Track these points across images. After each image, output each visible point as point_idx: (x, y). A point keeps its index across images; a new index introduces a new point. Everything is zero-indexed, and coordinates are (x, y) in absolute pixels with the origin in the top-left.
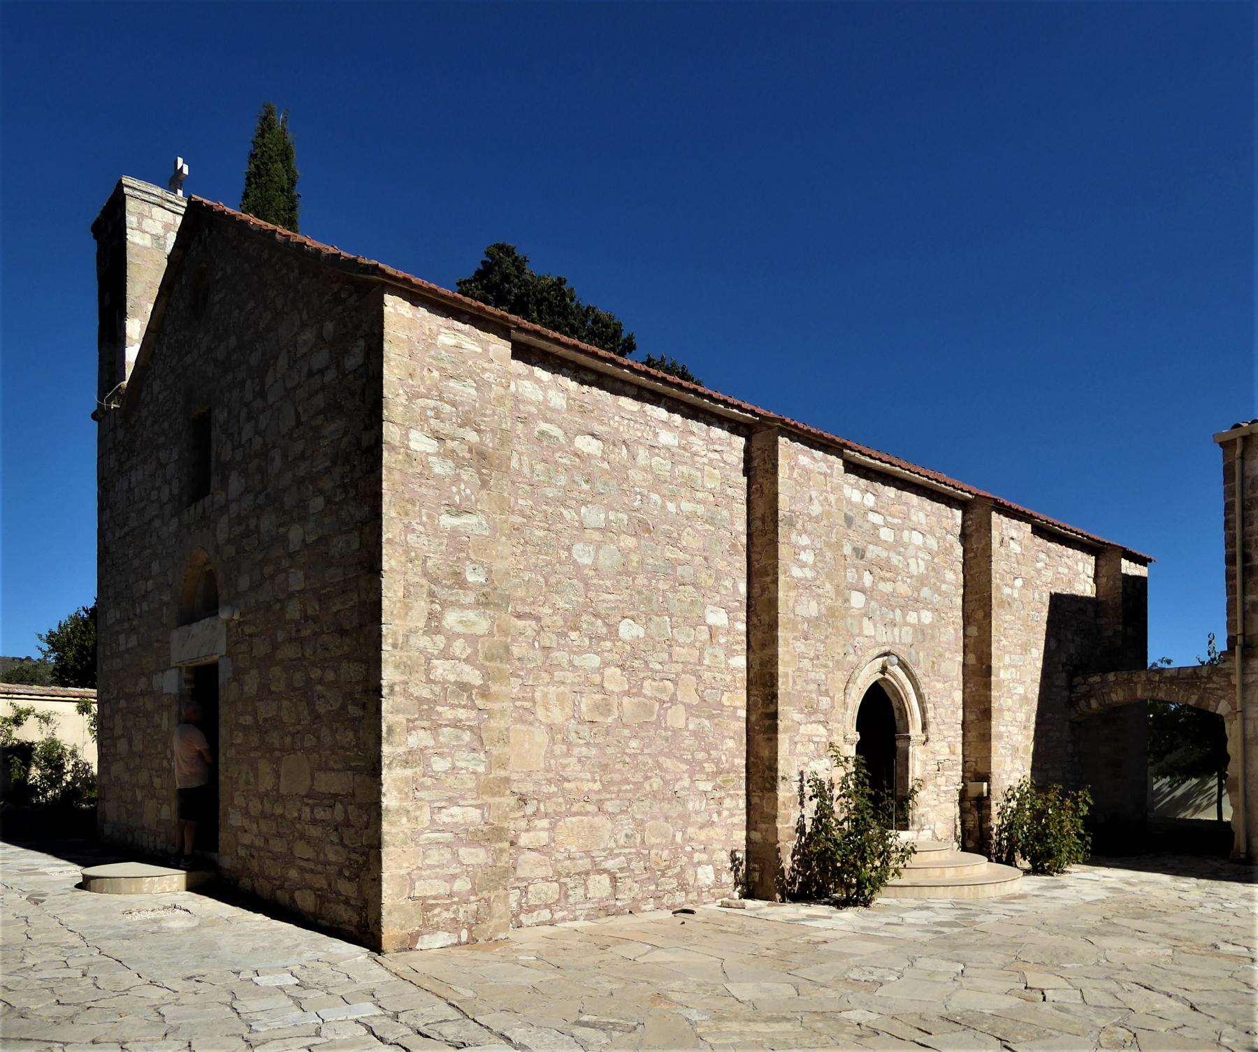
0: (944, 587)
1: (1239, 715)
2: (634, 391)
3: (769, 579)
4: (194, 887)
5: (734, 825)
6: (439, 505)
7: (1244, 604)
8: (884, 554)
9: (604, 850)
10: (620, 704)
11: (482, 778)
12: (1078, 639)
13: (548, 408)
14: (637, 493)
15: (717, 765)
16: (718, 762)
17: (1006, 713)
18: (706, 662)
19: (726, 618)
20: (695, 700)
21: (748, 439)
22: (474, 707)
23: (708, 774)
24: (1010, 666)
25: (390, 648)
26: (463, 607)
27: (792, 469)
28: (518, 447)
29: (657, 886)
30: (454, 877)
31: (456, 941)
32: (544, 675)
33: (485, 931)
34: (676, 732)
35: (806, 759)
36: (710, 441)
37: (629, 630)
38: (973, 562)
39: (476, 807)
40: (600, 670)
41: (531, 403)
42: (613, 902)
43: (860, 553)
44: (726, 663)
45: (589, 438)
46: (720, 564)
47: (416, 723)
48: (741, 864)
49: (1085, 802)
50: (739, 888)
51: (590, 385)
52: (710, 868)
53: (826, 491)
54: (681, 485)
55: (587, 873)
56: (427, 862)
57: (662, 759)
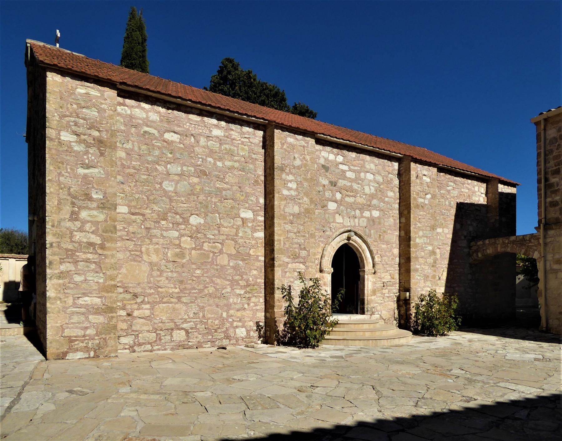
0: (386, 199)
1: (543, 258)
2: (198, 112)
4: (26, 334)
5: (257, 310)
6: (77, 164)
7: (545, 203)
8: (349, 184)
9: (181, 319)
10: (190, 254)
11: (101, 285)
12: (475, 224)
13: (149, 121)
14: (199, 158)
15: (247, 282)
16: (247, 281)
17: (420, 259)
18: (240, 235)
19: (252, 215)
20: (234, 252)
21: (265, 132)
22: (96, 253)
23: (241, 286)
24: (423, 236)
25: (50, 227)
26: (90, 209)
27: (283, 144)
28: (132, 139)
29: (213, 336)
30: (86, 328)
31: (88, 356)
32: (146, 240)
33: (104, 352)
35: (292, 280)
36: (242, 133)
37: (194, 220)
38: (403, 187)
39: (98, 297)
40: (179, 238)
41: (140, 119)
42: (187, 343)
43: (333, 184)
44: (252, 235)
45: (172, 134)
46: (248, 189)
47: (65, 260)
48: (262, 328)
49: (455, 301)
50: (262, 339)
51: (173, 109)
52: (244, 329)
53: (304, 154)
54: (225, 154)
55: (172, 329)
56: (71, 321)
57: (214, 279)
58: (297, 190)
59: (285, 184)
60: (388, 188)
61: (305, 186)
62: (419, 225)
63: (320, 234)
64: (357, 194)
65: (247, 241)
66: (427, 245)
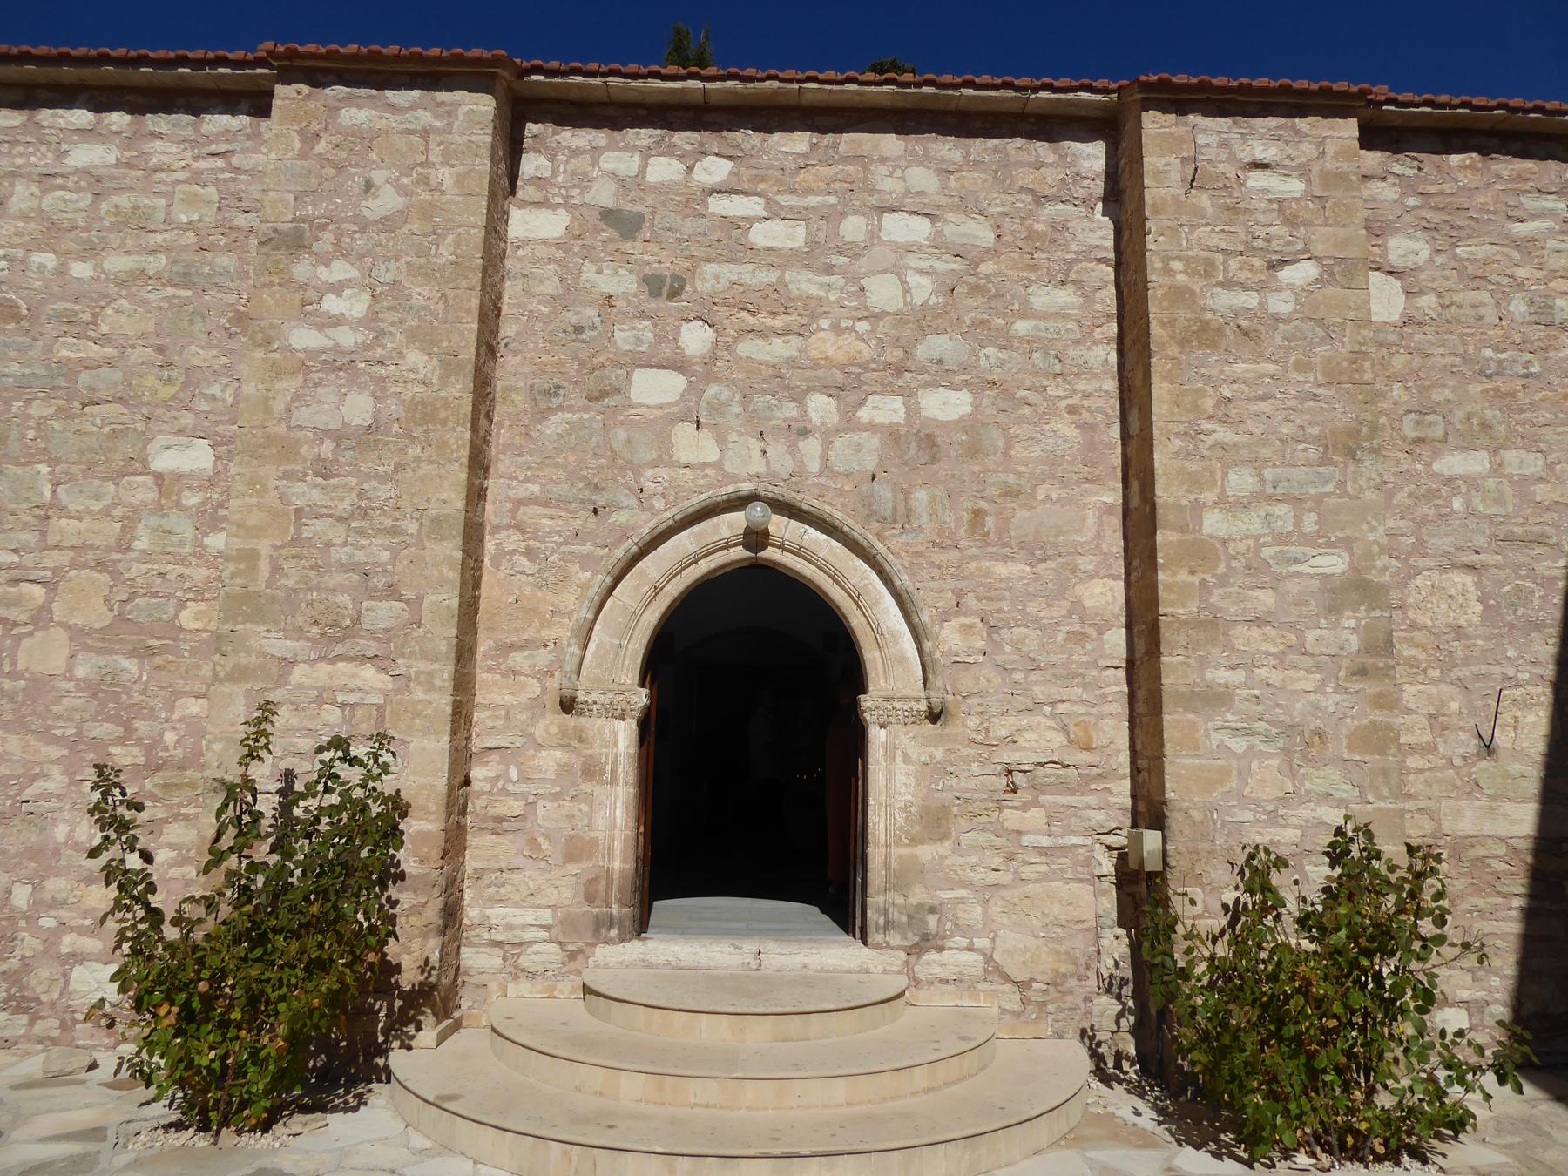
0: (1022, 327)
8: (766, 277)
15: (149, 750)
18: (142, 544)
24: (1259, 497)
34: (39, 684)
46: (198, 355)
58: (371, 320)
59: (304, 303)
60: (1033, 268)
61: (418, 301)
62: (1223, 434)
63: (576, 524)
64: (814, 316)
65: (173, 570)
66: (1295, 550)
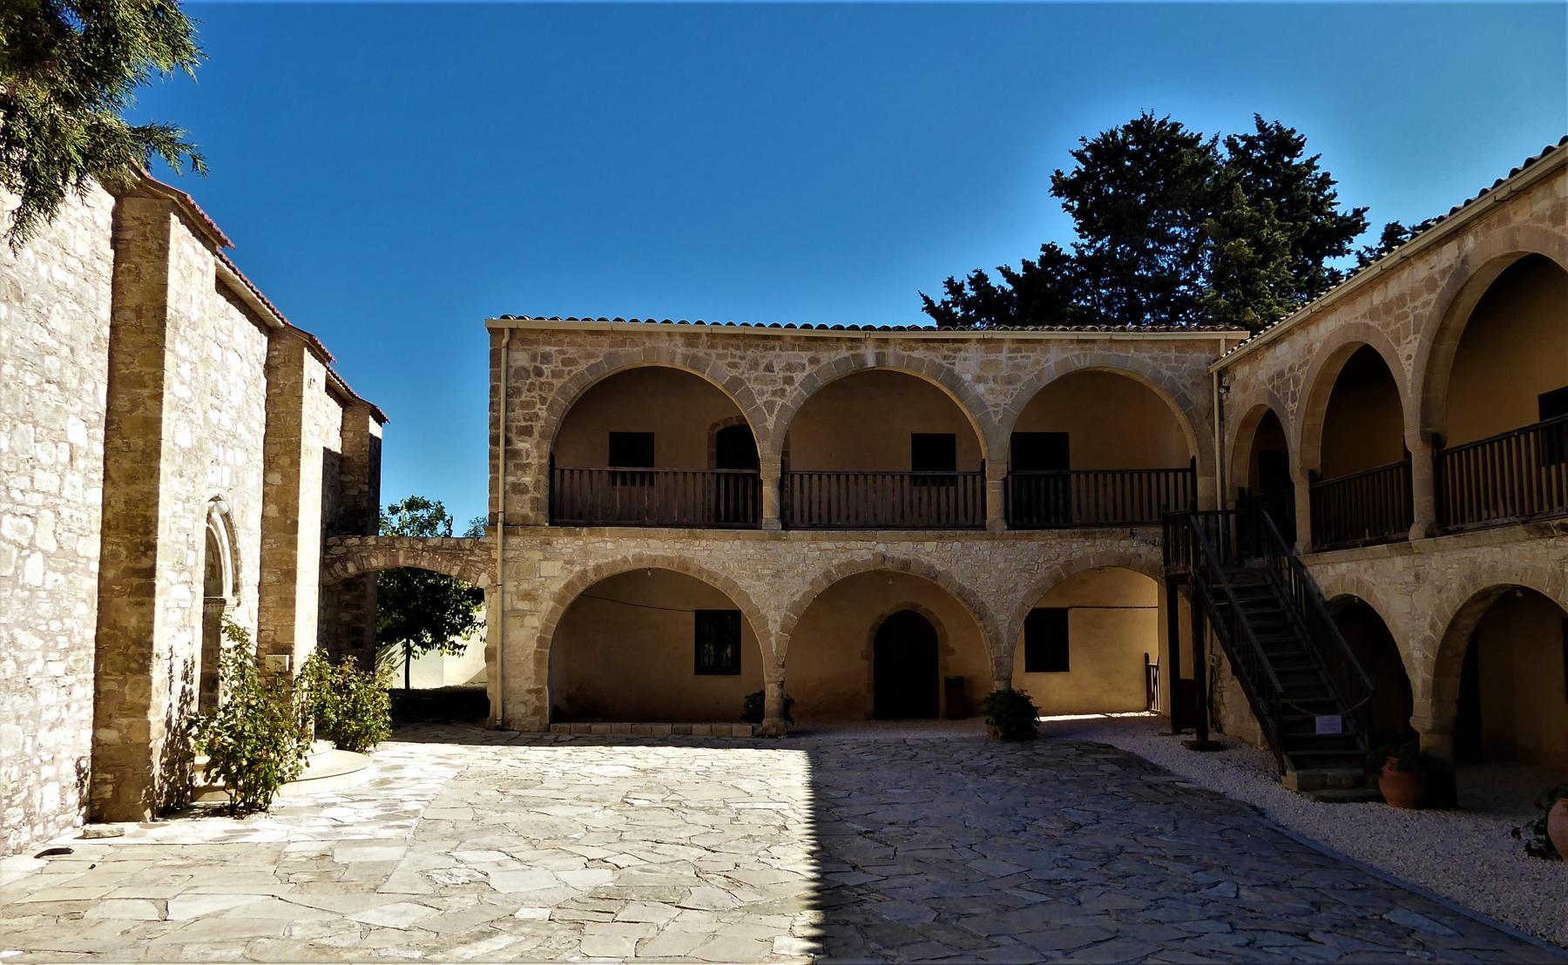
3: (146, 392)
50: (84, 810)
57: (17, 631)
